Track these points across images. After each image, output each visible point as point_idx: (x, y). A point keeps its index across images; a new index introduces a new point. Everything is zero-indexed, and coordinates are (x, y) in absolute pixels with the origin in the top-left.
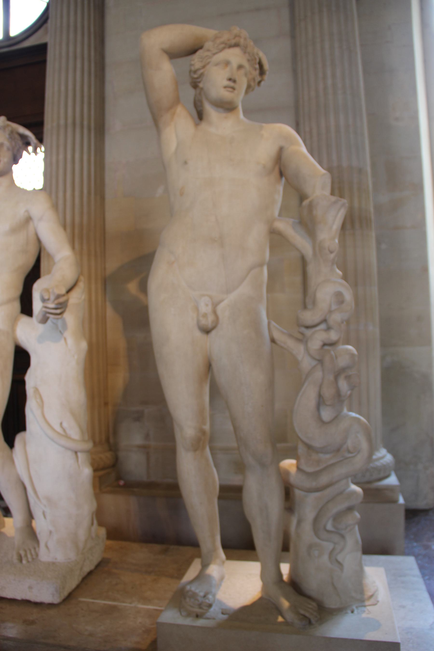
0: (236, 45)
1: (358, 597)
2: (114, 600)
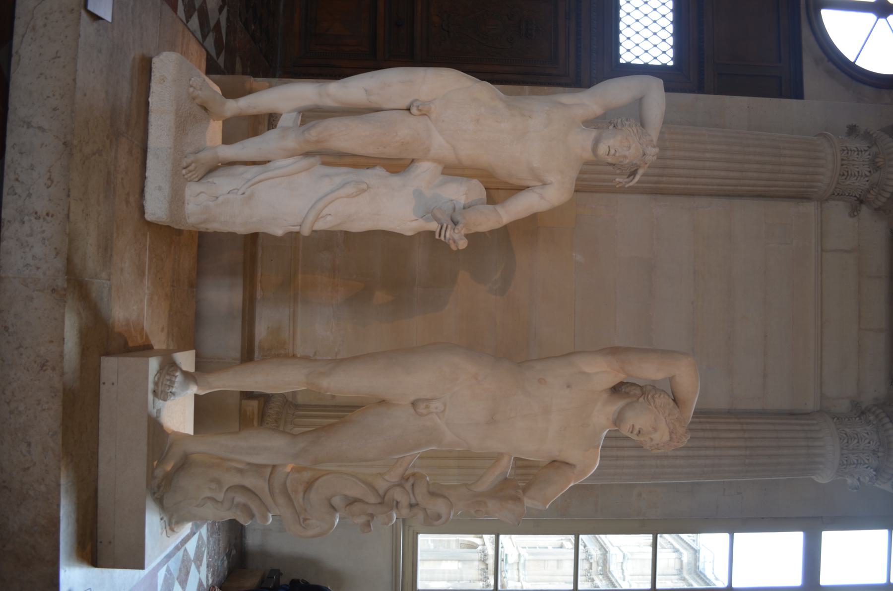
0: (671, 438)
1: (173, 521)
2: (150, 268)
